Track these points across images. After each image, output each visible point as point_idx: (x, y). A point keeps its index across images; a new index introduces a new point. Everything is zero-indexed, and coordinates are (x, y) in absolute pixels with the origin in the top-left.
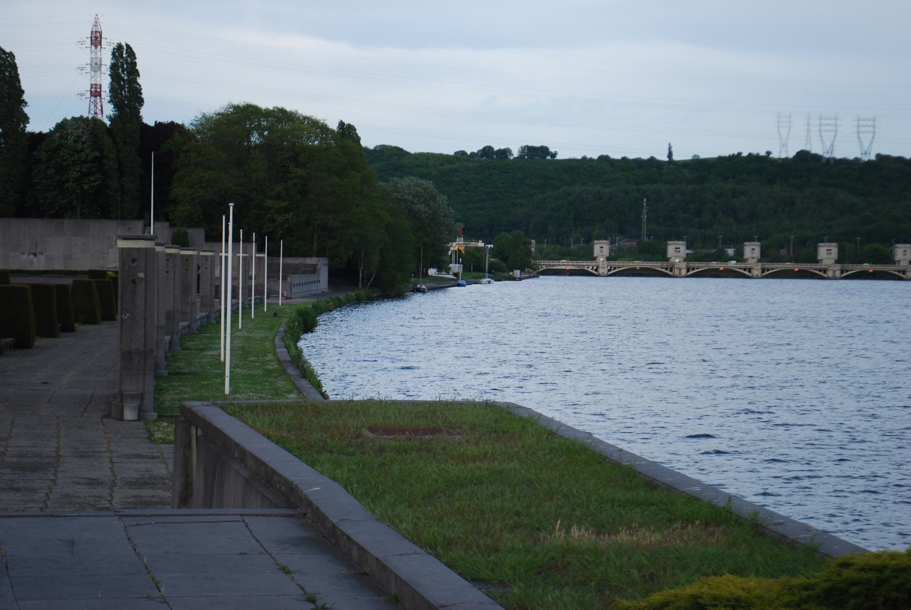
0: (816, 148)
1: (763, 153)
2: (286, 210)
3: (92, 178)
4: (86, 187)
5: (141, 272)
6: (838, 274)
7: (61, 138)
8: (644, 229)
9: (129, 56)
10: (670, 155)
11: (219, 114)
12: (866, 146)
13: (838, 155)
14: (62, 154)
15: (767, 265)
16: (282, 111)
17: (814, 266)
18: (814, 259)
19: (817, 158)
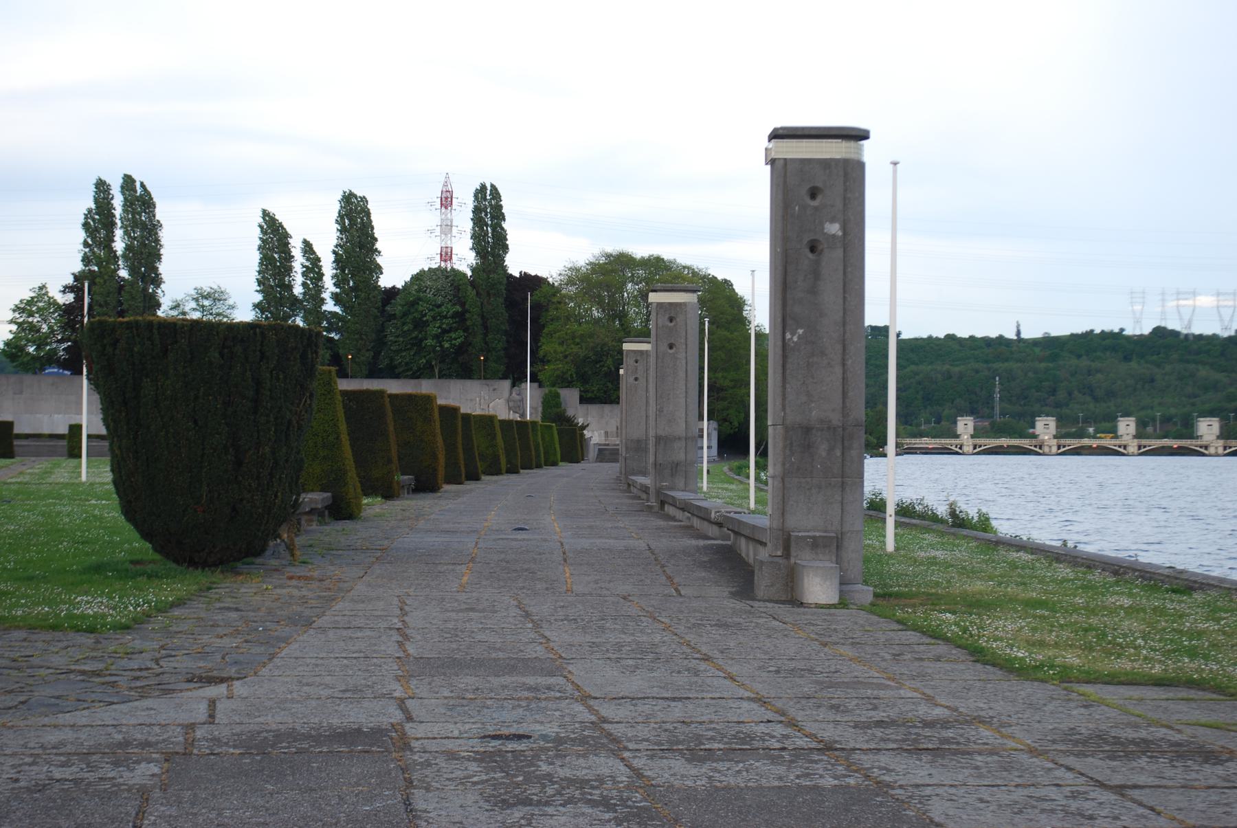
0: (1173, 324)
1: (1116, 330)
3: (453, 336)
4: (447, 345)
5: (833, 221)
6: (1220, 450)
7: (419, 291)
8: (997, 410)
9: (493, 198)
10: (1018, 333)
11: (591, 264)
12: (1227, 318)
13: (1197, 330)
14: (420, 308)
15: (1144, 442)
16: (659, 260)
17: (1194, 442)
19: (1175, 334)
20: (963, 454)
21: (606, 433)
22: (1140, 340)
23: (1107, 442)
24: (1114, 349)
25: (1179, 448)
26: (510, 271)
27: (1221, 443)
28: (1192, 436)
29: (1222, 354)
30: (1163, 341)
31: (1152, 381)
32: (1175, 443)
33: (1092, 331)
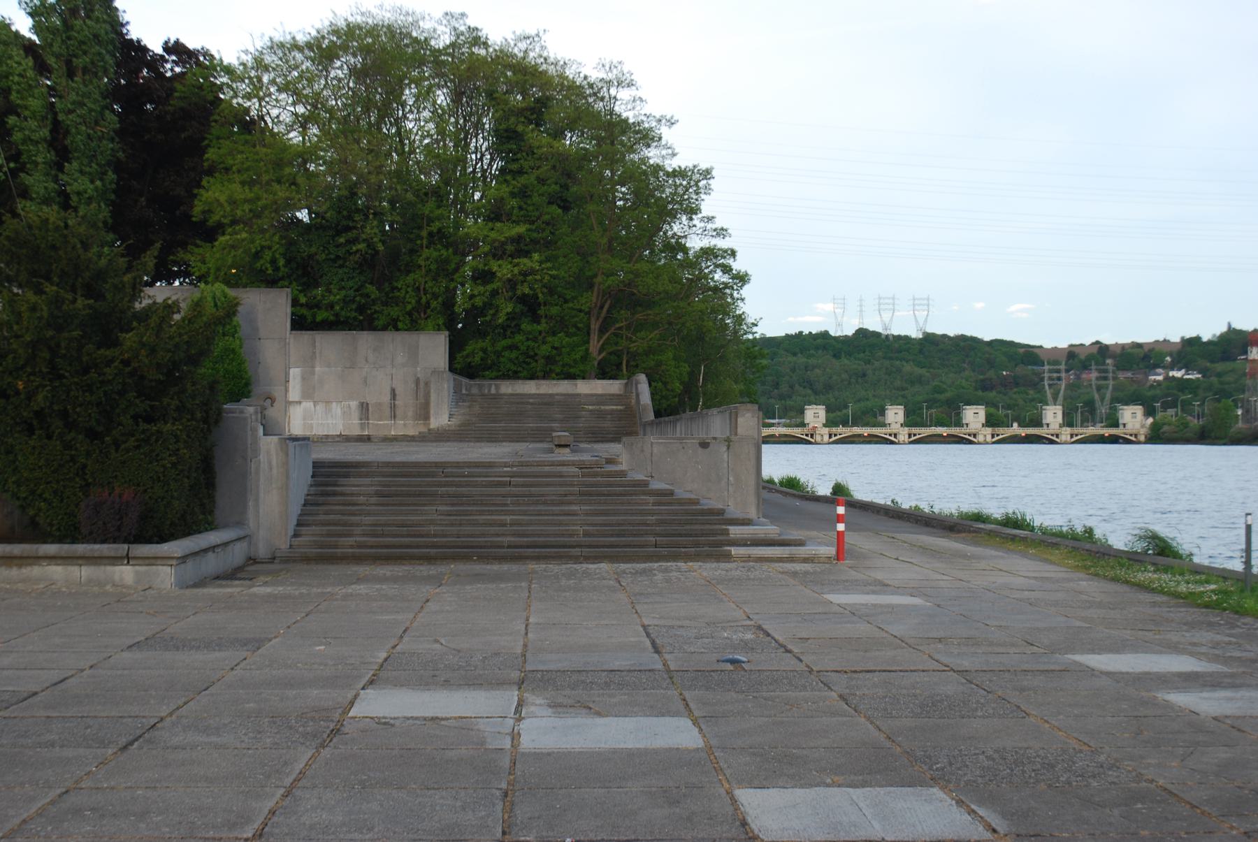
0: (873, 325)
2: (520, 248)
6: (989, 438)
12: (921, 322)
13: (896, 331)
15: (914, 430)
18: (1037, 422)
19: (876, 335)
20: (899, 443)
21: (364, 408)
22: (844, 340)
23: (797, 432)
24: (825, 348)
25: (780, 436)
26: (135, 32)
27: (989, 430)
28: (959, 423)
29: (921, 351)
30: (865, 341)
31: (864, 375)
32: (866, 431)
33: (801, 333)
